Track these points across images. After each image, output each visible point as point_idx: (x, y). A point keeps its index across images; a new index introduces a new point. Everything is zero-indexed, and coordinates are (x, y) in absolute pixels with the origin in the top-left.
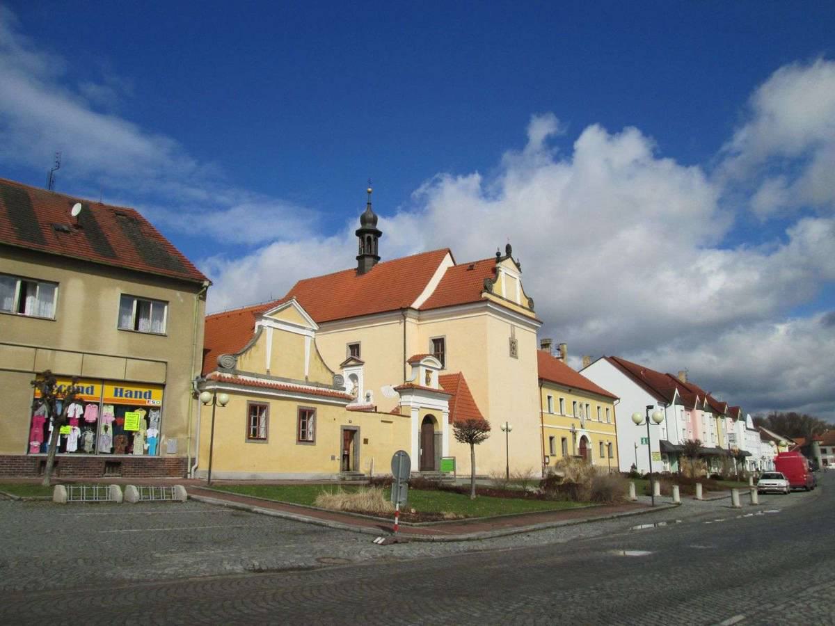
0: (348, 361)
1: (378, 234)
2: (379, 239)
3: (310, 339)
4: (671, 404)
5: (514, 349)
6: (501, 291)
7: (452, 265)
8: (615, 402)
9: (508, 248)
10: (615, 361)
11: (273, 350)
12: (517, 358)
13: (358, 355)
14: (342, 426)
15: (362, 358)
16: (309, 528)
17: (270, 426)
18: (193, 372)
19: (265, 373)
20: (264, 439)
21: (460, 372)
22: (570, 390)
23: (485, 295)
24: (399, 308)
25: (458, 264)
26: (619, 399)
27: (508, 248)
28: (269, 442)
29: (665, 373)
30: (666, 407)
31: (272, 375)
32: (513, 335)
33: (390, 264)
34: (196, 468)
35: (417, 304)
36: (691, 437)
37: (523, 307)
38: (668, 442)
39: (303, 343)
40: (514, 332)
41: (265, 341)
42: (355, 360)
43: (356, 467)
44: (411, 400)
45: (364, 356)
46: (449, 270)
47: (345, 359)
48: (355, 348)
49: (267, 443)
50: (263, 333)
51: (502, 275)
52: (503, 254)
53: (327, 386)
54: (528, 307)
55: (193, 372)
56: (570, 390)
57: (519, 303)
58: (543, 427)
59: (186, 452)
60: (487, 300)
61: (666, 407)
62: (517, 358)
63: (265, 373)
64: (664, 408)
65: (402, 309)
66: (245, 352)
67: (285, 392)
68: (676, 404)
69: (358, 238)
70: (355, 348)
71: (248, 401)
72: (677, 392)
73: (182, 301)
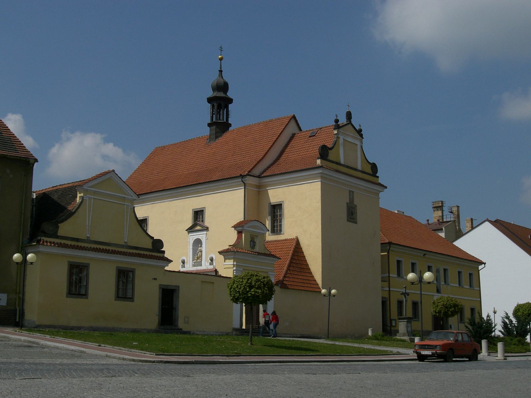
1: (230, 101)
2: (230, 106)
6: (338, 156)
9: (349, 115)
10: (499, 224)
12: (356, 223)
13: (203, 221)
14: (160, 285)
15: (207, 223)
16: (26, 344)
17: (90, 285)
21: (235, 227)
24: (239, 175)
26: (485, 264)
27: (349, 115)
28: (89, 297)
32: (352, 200)
40: (353, 196)
42: (200, 226)
43: (230, 333)
45: (208, 221)
48: (198, 214)
49: (87, 298)
52: (343, 120)
57: (359, 168)
58: (389, 290)
62: (356, 223)
66: (66, 219)
69: (209, 105)
70: (198, 214)
71: (69, 262)
73: (11, 176)
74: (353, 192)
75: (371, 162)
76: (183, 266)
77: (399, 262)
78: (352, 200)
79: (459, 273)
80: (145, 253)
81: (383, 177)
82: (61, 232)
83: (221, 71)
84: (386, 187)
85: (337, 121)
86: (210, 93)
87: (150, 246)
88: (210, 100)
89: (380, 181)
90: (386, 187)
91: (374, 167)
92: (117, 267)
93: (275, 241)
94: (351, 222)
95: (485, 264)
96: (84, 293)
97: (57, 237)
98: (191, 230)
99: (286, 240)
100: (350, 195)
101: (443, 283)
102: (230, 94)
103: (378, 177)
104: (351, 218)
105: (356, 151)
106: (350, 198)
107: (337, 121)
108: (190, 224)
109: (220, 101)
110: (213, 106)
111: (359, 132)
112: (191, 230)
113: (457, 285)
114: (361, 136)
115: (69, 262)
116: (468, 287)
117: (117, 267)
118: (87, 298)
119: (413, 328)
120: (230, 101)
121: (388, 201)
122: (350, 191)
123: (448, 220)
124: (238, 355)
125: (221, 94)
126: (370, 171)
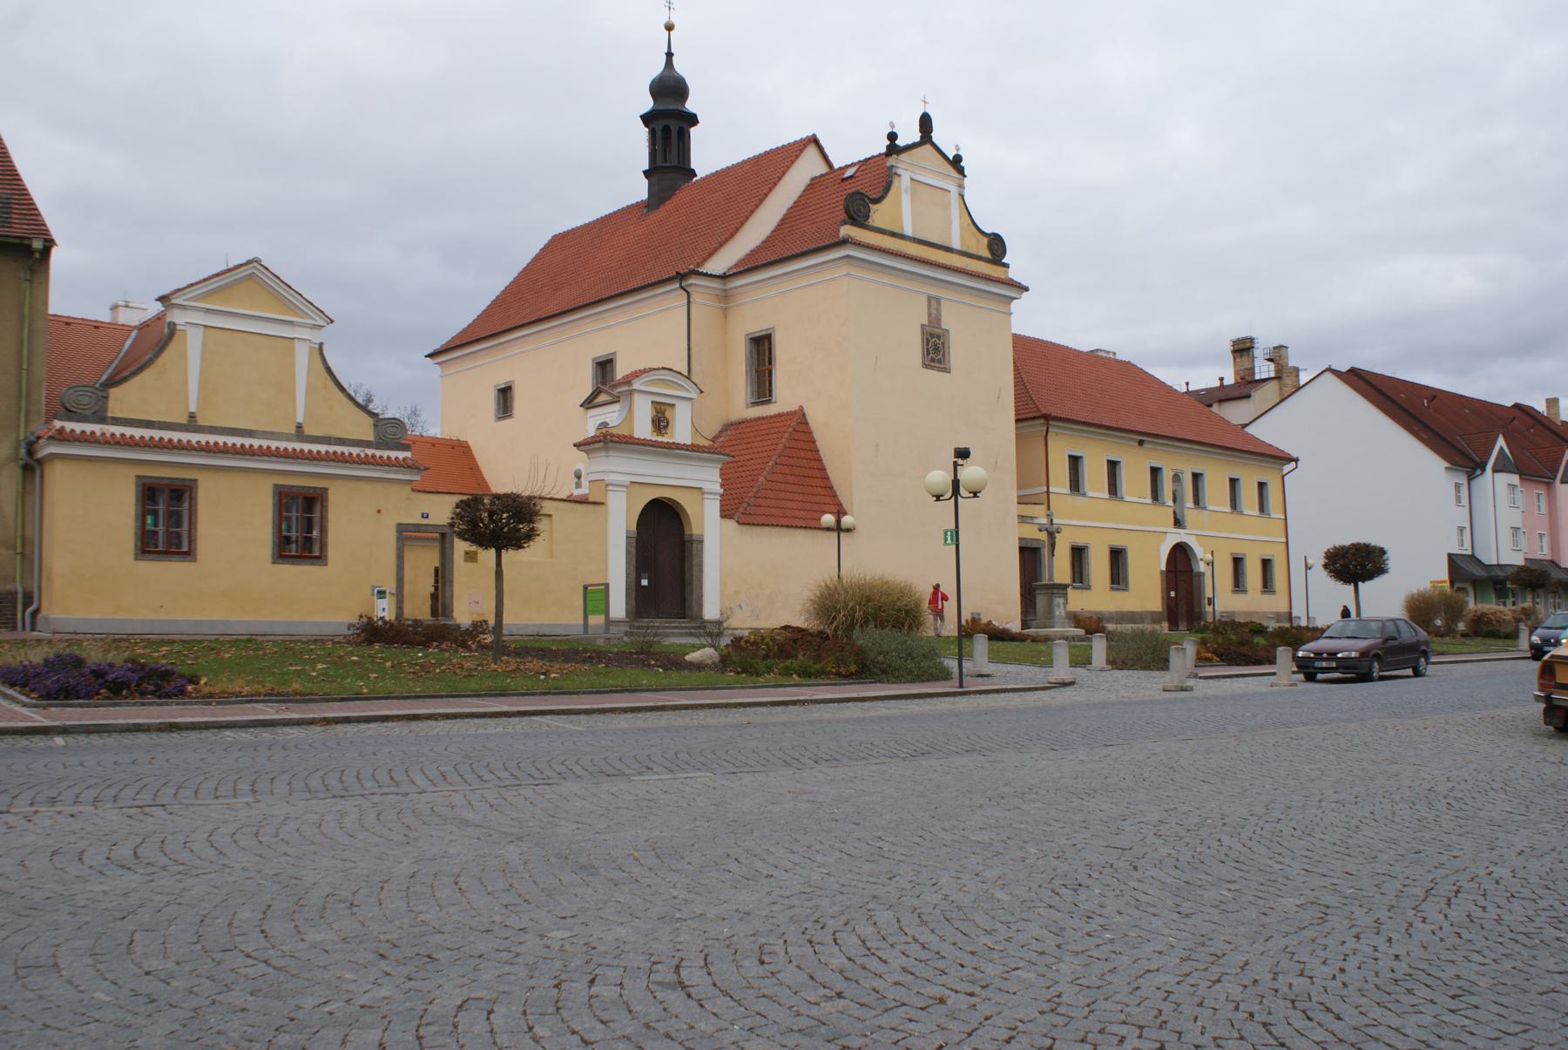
0: (596, 393)
1: (692, 120)
3: (307, 345)
4: (1483, 470)
5: (936, 349)
7: (823, 169)
8: (1287, 468)
9: (926, 123)
11: (203, 370)
12: (947, 370)
18: (22, 425)
19: (292, 430)
20: (319, 558)
21: (801, 408)
22: (1141, 443)
23: (846, 230)
25: (836, 166)
27: (926, 123)
29: (1509, 404)
30: (1470, 478)
31: (201, 422)
32: (935, 319)
33: (703, 179)
34: (37, 611)
35: (719, 263)
36: (1543, 553)
37: (980, 258)
38: (1473, 558)
39: (291, 353)
41: (183, 356)
44: (618, 468)
46: (815, 182)
47: (588, 391)
49: (195, 560)
50: (176, 339)
51: (903, 182)
53: (367, 444)
54: (987, 254)
55: (22, 425)
56: (1141, 443)
59: (14, 580)
60: (844, 242)
61: (1470, 478)
63: (184, 420)
64: (1463, 479)
65: (681, 277)
67: (240, 453)
68: (1495, 471)
71: (138, 477)
72: (1501, 442)
74: (938, 300)
75: (988, 230)
76: (578, 485)
77: (1075, 461)
78: (935, 319)
79: (1233, 482)
80: (355, 451)
81: (1018, 264)
82: (114, 410)
83: (669, 55)
84: (1026, 289)
85: (892, 137)
86: (648, 104)
87: (369, 435)
88: (647, 119)
89: (1014, 274)
90: (1026, 289)
91: (997, 246)
92: (276, 486)
93: (759, 419)
94: (933, 368)
95: (1296, 460)
96: (185, 549)
97: (103, 420)
98: (589, 404)
99: (780, 415)
100: (929, 306)
101: (1189, 503)
102: (691, 105)
103: (1006, 266)
104: (933, 360)
105: (948, 206)
106: (930, 315)
107: (892, 137)
108: (588, 391)
109: (669, 118)
110: (652, 133)
111: (956, 162)
112: (589, 404)
113: (1228, 509)
114: (961, 171)
115: (138, 477)
116: (1256, 512)
117: (276, 486)
118: (195, 560)
119: (1351, 587)
120: (692, 120)
121: (1032, 318)
122: (930, 299)
123: (1265, 376)
124: (502, 693)
125: (669, 105)
126: (986, 254)
